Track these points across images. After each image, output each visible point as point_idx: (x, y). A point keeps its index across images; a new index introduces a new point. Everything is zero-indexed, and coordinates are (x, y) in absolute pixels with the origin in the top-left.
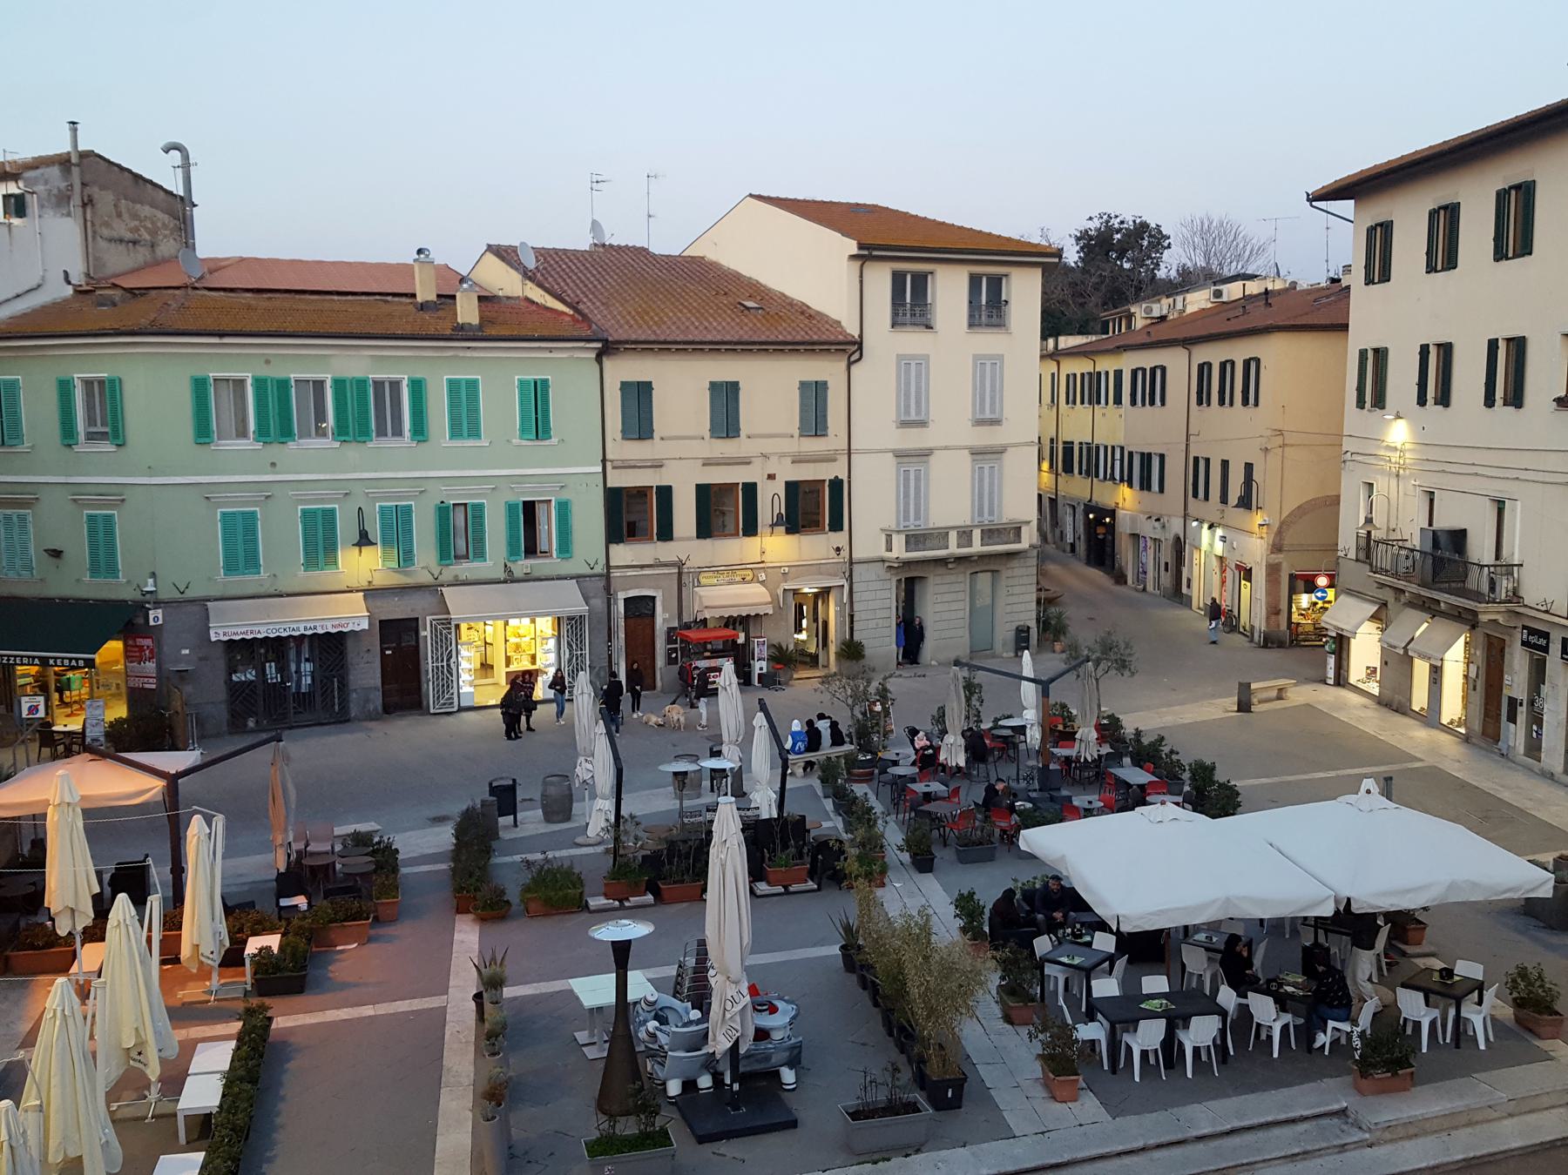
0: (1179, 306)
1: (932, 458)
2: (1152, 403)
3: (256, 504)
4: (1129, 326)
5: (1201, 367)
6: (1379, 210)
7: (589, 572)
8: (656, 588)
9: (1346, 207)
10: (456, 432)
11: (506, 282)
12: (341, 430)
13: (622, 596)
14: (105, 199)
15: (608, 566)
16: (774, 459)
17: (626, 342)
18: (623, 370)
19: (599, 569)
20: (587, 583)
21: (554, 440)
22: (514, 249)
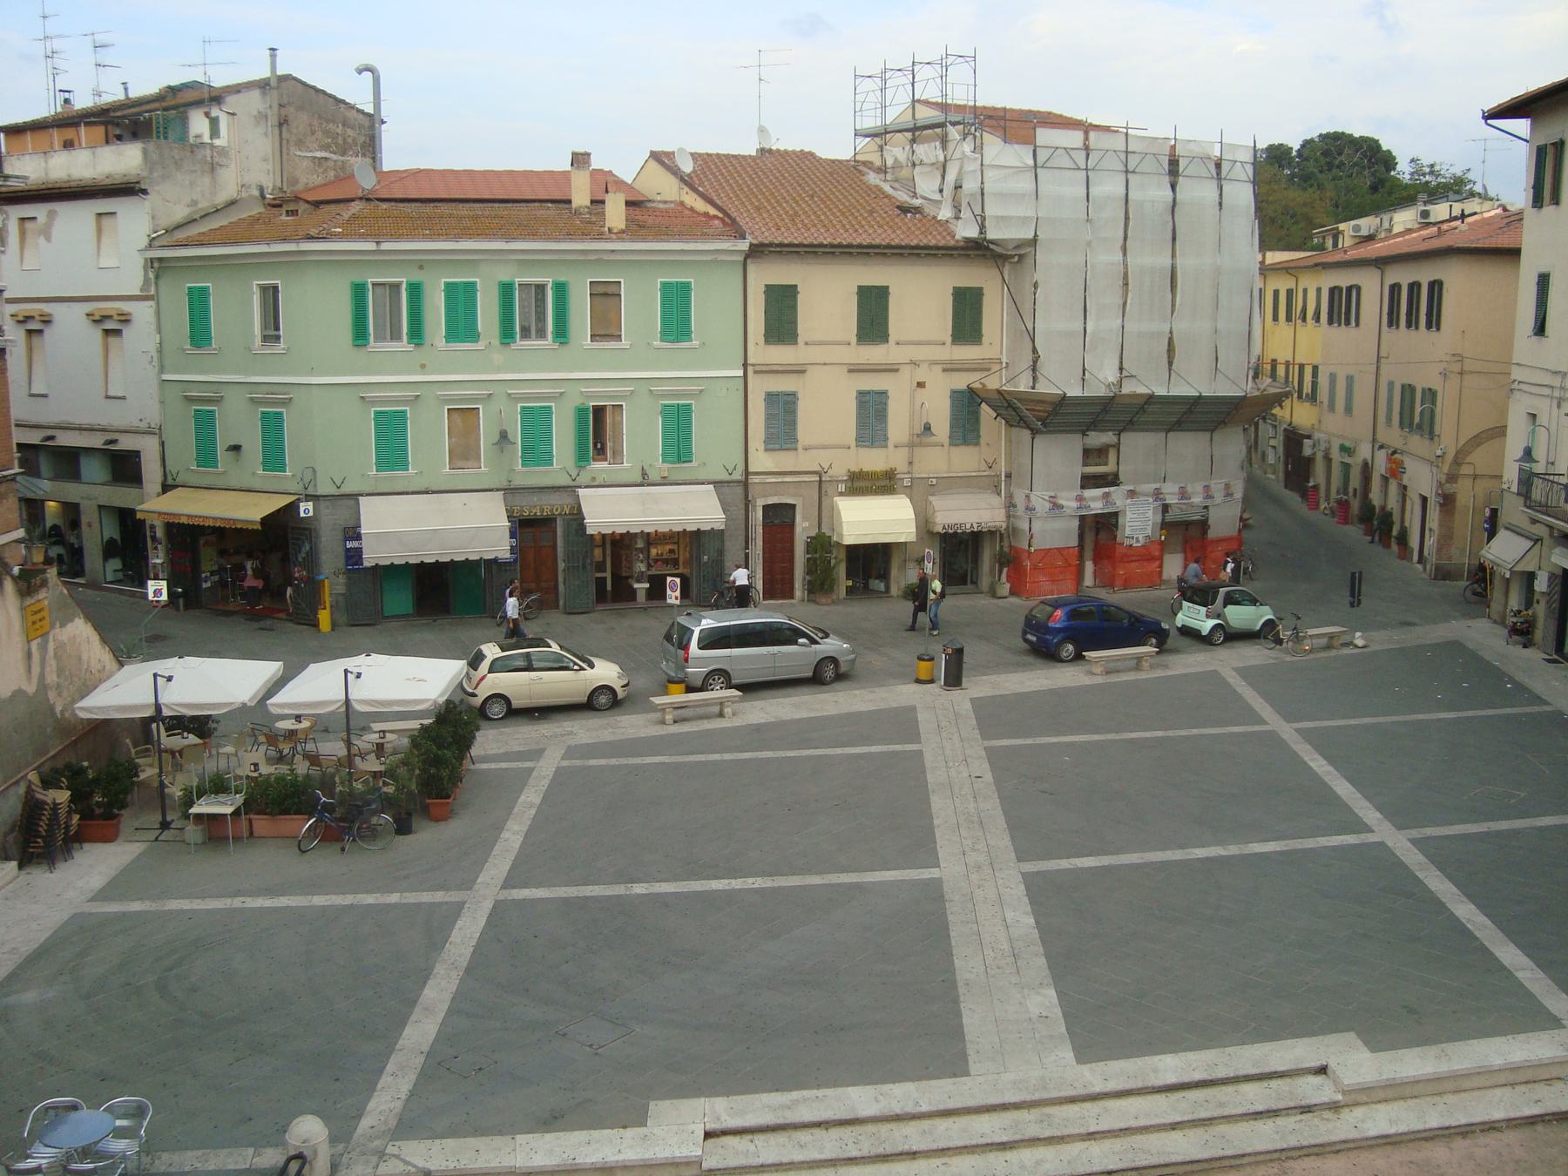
0: (1386, 225)
1: (808, 374)
2: (1348, 323)
3: (406, 402)
4: (1335, 244)
7: (728, 478)
8: (794, 495)
9: (1521, 126)
10: (452, 335)
11: (664, 188)
12: (1412, 388)
13: (760, 503)
14: (301, 121)
15: (747, 473)
16: (924, 367)
17: (770, 245)
18: (764, 275)
19: (738, 476)
20: (726, 490)
21: (695, 343)
22: (670, 155)
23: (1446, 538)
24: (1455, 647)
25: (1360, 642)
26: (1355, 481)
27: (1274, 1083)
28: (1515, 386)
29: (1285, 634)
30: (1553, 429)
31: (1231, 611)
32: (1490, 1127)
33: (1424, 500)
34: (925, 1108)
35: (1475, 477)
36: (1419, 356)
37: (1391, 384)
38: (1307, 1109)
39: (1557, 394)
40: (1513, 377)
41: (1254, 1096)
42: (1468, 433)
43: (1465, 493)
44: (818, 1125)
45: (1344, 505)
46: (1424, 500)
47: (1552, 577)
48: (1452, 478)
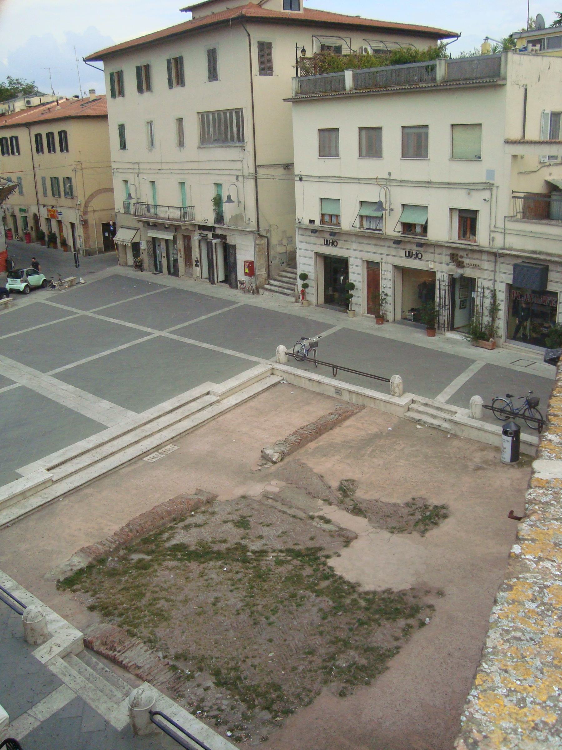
0: (12, 108)
2: (13, 153)
5: (36, 136)
6: (115, 67)
9: (100, 64)
23: (87, 238)
24: (116, 277)
25: (83, 281)
26: (31, 223)
27: (198, 401)
28: (115, 170)
29: (55, 283)
30: (137, 185)
31: (30, 278)
32: (259, 394)
33: (73, 225)
34: (107, 439)
35: (94, 211)
36: (56, 164)
37: (43, 179)
38: (211, 404)
39: (136, 171)
40: (113, 167)
41: (195, 406)
42: (88, 194)
43: (92, 219)
44: (76, 456)
45: (28, 235)
46: (73, 225)
47: (148, 242)
48: (85, 213)
